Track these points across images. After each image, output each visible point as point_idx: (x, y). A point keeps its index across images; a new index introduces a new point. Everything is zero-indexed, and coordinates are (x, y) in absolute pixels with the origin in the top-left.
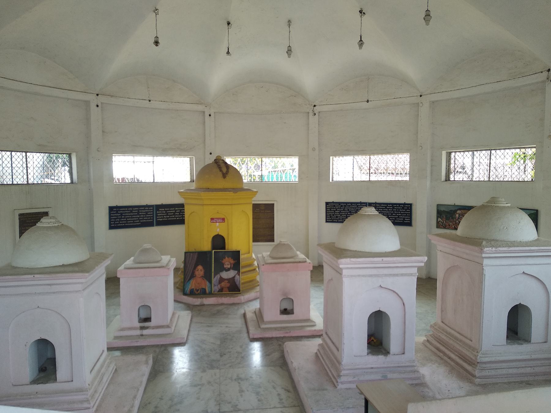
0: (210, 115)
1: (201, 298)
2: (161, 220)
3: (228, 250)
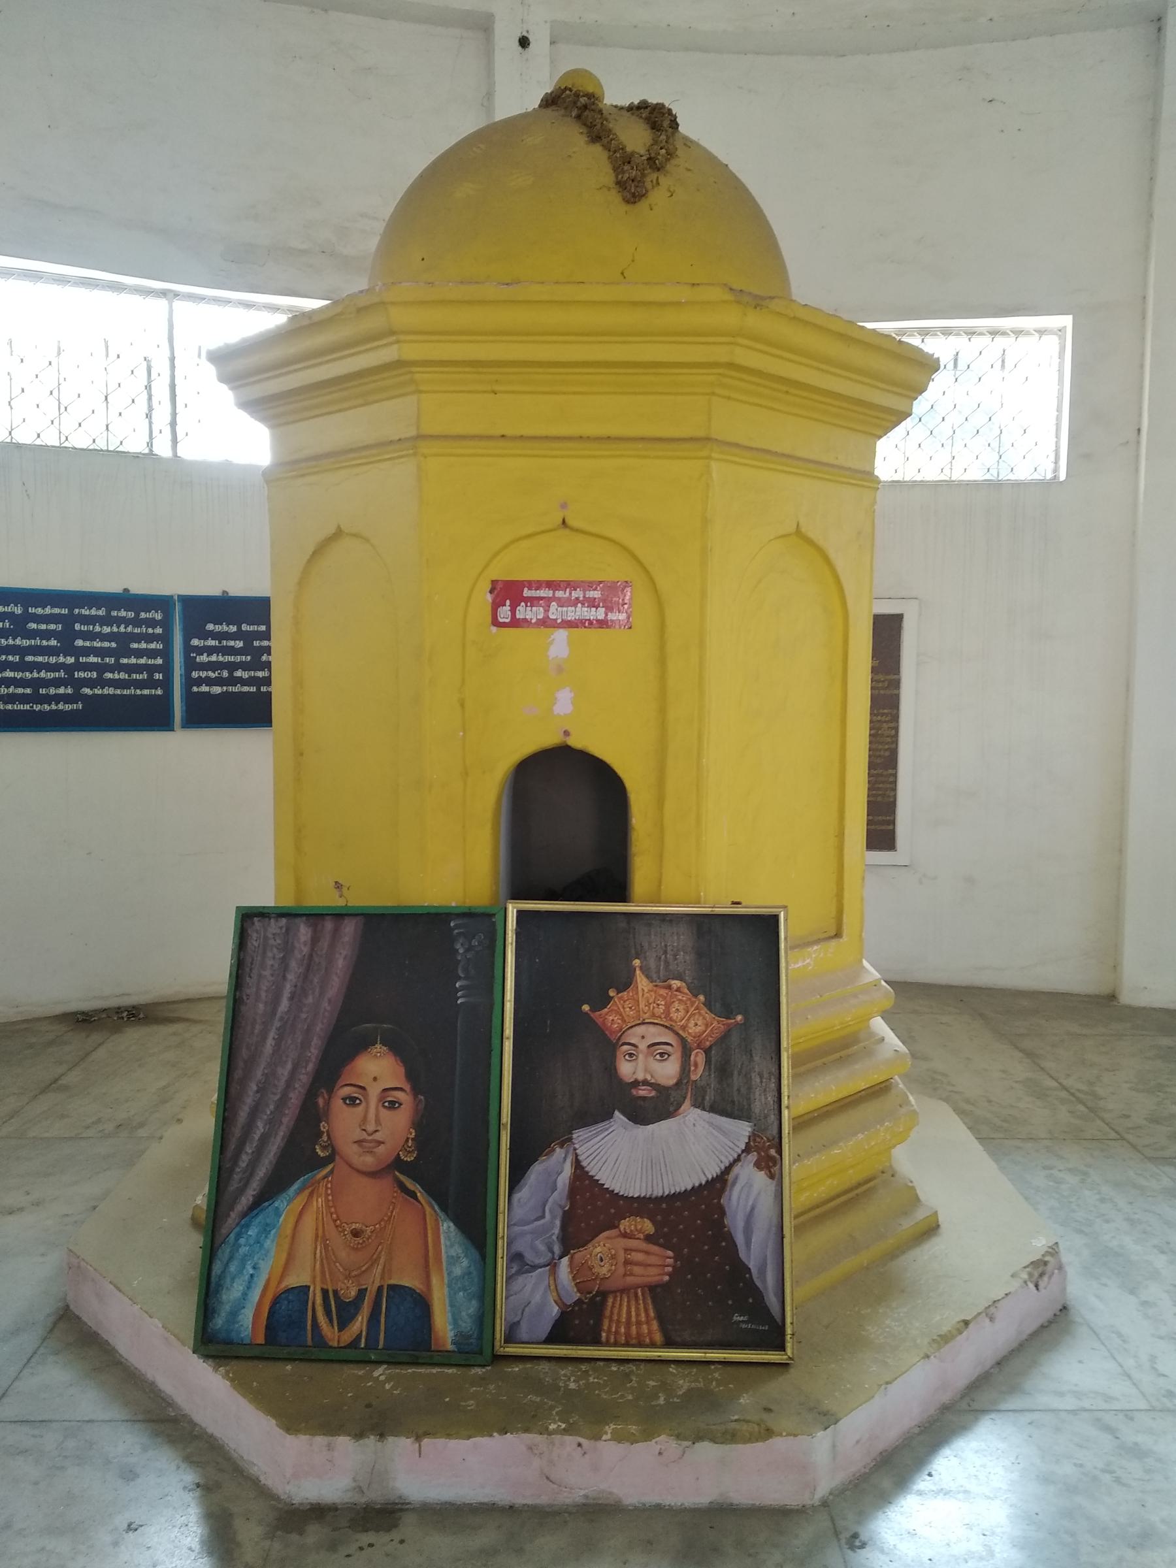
0: (524, 42)
1: (359, 1435)
2: (217, 690)
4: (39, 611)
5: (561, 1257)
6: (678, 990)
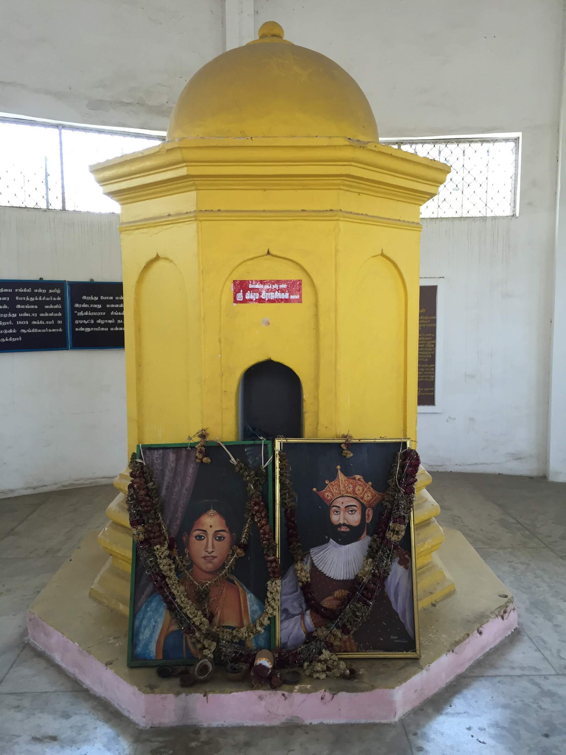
2: (88, 330)
3: (315, 435)
4: (21, 290)
5: (306, 610)
6: (359, 480)
